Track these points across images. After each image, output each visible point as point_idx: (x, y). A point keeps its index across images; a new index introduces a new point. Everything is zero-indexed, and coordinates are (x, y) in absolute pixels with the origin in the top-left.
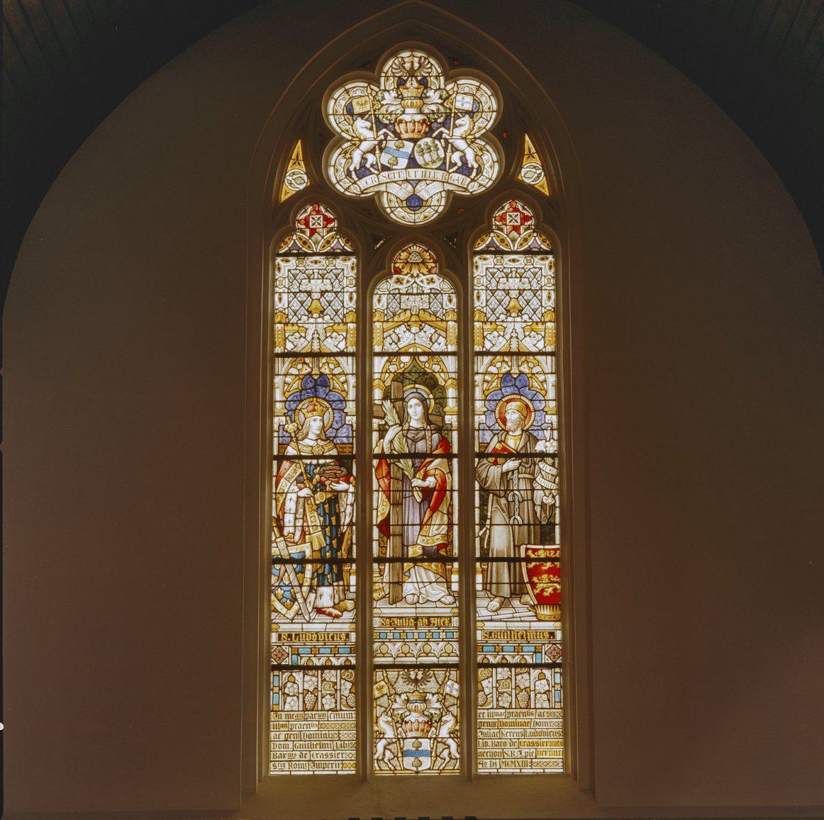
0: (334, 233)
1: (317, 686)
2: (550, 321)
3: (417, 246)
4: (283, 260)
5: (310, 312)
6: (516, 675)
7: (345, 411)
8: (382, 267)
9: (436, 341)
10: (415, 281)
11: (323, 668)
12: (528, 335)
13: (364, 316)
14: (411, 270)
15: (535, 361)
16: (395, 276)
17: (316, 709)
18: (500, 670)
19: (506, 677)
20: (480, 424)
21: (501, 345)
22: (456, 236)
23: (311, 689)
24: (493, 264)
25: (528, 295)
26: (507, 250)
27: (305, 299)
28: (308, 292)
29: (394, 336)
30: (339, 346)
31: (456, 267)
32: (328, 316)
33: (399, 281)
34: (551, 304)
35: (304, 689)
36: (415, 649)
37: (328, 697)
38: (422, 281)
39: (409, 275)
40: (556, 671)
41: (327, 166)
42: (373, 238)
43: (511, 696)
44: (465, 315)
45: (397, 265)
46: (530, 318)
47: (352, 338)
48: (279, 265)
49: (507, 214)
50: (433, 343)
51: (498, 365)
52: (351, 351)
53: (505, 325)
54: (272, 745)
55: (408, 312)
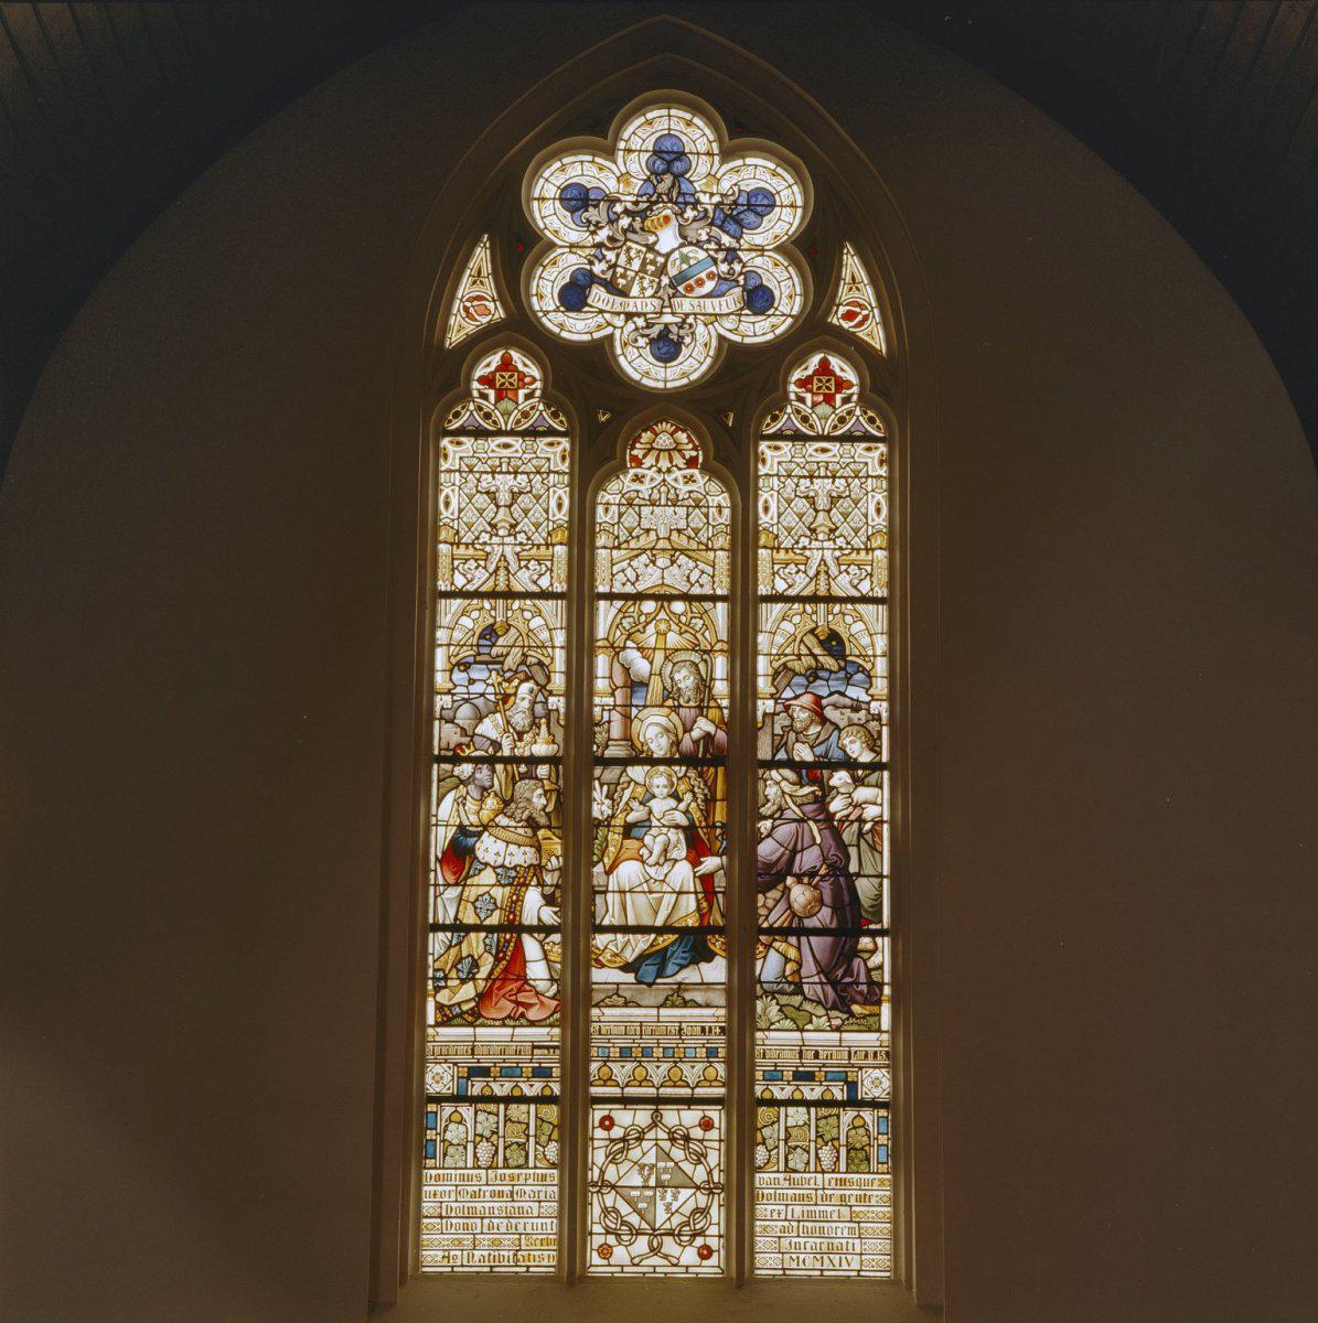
0: (854, 404)
1: (497, 1128)
2: (561, 544)
3: (667, 423)
4: (452, 442)
5: (493, 526)
6: (817, 1120)
7: (548, 688)
8: (612, 457)
9: (697, 581)
10: (662, 486)
11: (508, 1100)
12: (846, 570)
13: (581, 534)
14: (657, 460)
15: (854, 614)
16: (632, 472)
17: (494, 1165)
18: (791, 1110)
19: (801, 1123)
20: (442, 709)
21: (480, 579)
22: (732, 410)
23: (487, 1133)
24: (790, 457)
25: (525, 500)
26: (811, 433)
27: (485, 505)
28: (492, 489)
29: (629, 572)
30: (539, 582)
31: (731, 461)
32: (842, 539)
33: (638, 479)
34: (880, 521)
35: (476, 1135)
36: (658, 1072)
37: (515, 1146)
38: (676, 480)
39: (654, 469)
40: (880, 1114)
41: (529, 296)
42: (597, 410)
43: (808, 1152)
44: (744, 537)
45: (635, 452)
46: (848, 543)
47: (561, 569)
48: (876, 448)
49: (815, 378)
50: (692, 585)
51: (797, 619)
52: (559, 590)
53: (807, 553)
54: (554, 1228)
55: (653, 534)
